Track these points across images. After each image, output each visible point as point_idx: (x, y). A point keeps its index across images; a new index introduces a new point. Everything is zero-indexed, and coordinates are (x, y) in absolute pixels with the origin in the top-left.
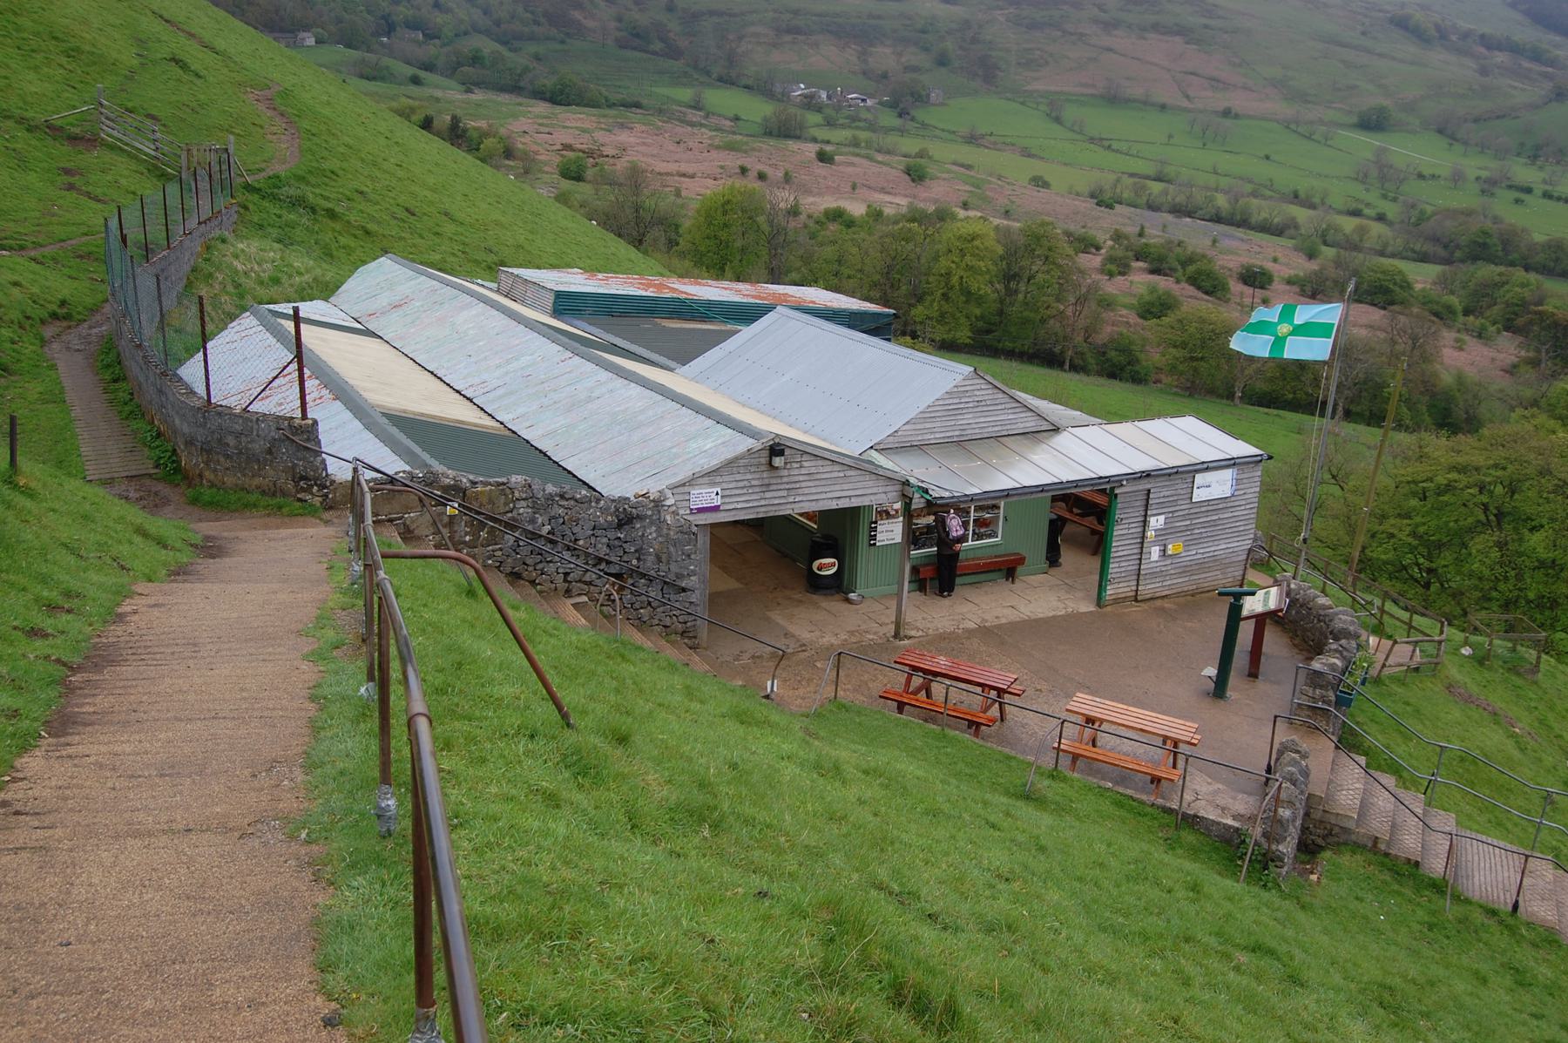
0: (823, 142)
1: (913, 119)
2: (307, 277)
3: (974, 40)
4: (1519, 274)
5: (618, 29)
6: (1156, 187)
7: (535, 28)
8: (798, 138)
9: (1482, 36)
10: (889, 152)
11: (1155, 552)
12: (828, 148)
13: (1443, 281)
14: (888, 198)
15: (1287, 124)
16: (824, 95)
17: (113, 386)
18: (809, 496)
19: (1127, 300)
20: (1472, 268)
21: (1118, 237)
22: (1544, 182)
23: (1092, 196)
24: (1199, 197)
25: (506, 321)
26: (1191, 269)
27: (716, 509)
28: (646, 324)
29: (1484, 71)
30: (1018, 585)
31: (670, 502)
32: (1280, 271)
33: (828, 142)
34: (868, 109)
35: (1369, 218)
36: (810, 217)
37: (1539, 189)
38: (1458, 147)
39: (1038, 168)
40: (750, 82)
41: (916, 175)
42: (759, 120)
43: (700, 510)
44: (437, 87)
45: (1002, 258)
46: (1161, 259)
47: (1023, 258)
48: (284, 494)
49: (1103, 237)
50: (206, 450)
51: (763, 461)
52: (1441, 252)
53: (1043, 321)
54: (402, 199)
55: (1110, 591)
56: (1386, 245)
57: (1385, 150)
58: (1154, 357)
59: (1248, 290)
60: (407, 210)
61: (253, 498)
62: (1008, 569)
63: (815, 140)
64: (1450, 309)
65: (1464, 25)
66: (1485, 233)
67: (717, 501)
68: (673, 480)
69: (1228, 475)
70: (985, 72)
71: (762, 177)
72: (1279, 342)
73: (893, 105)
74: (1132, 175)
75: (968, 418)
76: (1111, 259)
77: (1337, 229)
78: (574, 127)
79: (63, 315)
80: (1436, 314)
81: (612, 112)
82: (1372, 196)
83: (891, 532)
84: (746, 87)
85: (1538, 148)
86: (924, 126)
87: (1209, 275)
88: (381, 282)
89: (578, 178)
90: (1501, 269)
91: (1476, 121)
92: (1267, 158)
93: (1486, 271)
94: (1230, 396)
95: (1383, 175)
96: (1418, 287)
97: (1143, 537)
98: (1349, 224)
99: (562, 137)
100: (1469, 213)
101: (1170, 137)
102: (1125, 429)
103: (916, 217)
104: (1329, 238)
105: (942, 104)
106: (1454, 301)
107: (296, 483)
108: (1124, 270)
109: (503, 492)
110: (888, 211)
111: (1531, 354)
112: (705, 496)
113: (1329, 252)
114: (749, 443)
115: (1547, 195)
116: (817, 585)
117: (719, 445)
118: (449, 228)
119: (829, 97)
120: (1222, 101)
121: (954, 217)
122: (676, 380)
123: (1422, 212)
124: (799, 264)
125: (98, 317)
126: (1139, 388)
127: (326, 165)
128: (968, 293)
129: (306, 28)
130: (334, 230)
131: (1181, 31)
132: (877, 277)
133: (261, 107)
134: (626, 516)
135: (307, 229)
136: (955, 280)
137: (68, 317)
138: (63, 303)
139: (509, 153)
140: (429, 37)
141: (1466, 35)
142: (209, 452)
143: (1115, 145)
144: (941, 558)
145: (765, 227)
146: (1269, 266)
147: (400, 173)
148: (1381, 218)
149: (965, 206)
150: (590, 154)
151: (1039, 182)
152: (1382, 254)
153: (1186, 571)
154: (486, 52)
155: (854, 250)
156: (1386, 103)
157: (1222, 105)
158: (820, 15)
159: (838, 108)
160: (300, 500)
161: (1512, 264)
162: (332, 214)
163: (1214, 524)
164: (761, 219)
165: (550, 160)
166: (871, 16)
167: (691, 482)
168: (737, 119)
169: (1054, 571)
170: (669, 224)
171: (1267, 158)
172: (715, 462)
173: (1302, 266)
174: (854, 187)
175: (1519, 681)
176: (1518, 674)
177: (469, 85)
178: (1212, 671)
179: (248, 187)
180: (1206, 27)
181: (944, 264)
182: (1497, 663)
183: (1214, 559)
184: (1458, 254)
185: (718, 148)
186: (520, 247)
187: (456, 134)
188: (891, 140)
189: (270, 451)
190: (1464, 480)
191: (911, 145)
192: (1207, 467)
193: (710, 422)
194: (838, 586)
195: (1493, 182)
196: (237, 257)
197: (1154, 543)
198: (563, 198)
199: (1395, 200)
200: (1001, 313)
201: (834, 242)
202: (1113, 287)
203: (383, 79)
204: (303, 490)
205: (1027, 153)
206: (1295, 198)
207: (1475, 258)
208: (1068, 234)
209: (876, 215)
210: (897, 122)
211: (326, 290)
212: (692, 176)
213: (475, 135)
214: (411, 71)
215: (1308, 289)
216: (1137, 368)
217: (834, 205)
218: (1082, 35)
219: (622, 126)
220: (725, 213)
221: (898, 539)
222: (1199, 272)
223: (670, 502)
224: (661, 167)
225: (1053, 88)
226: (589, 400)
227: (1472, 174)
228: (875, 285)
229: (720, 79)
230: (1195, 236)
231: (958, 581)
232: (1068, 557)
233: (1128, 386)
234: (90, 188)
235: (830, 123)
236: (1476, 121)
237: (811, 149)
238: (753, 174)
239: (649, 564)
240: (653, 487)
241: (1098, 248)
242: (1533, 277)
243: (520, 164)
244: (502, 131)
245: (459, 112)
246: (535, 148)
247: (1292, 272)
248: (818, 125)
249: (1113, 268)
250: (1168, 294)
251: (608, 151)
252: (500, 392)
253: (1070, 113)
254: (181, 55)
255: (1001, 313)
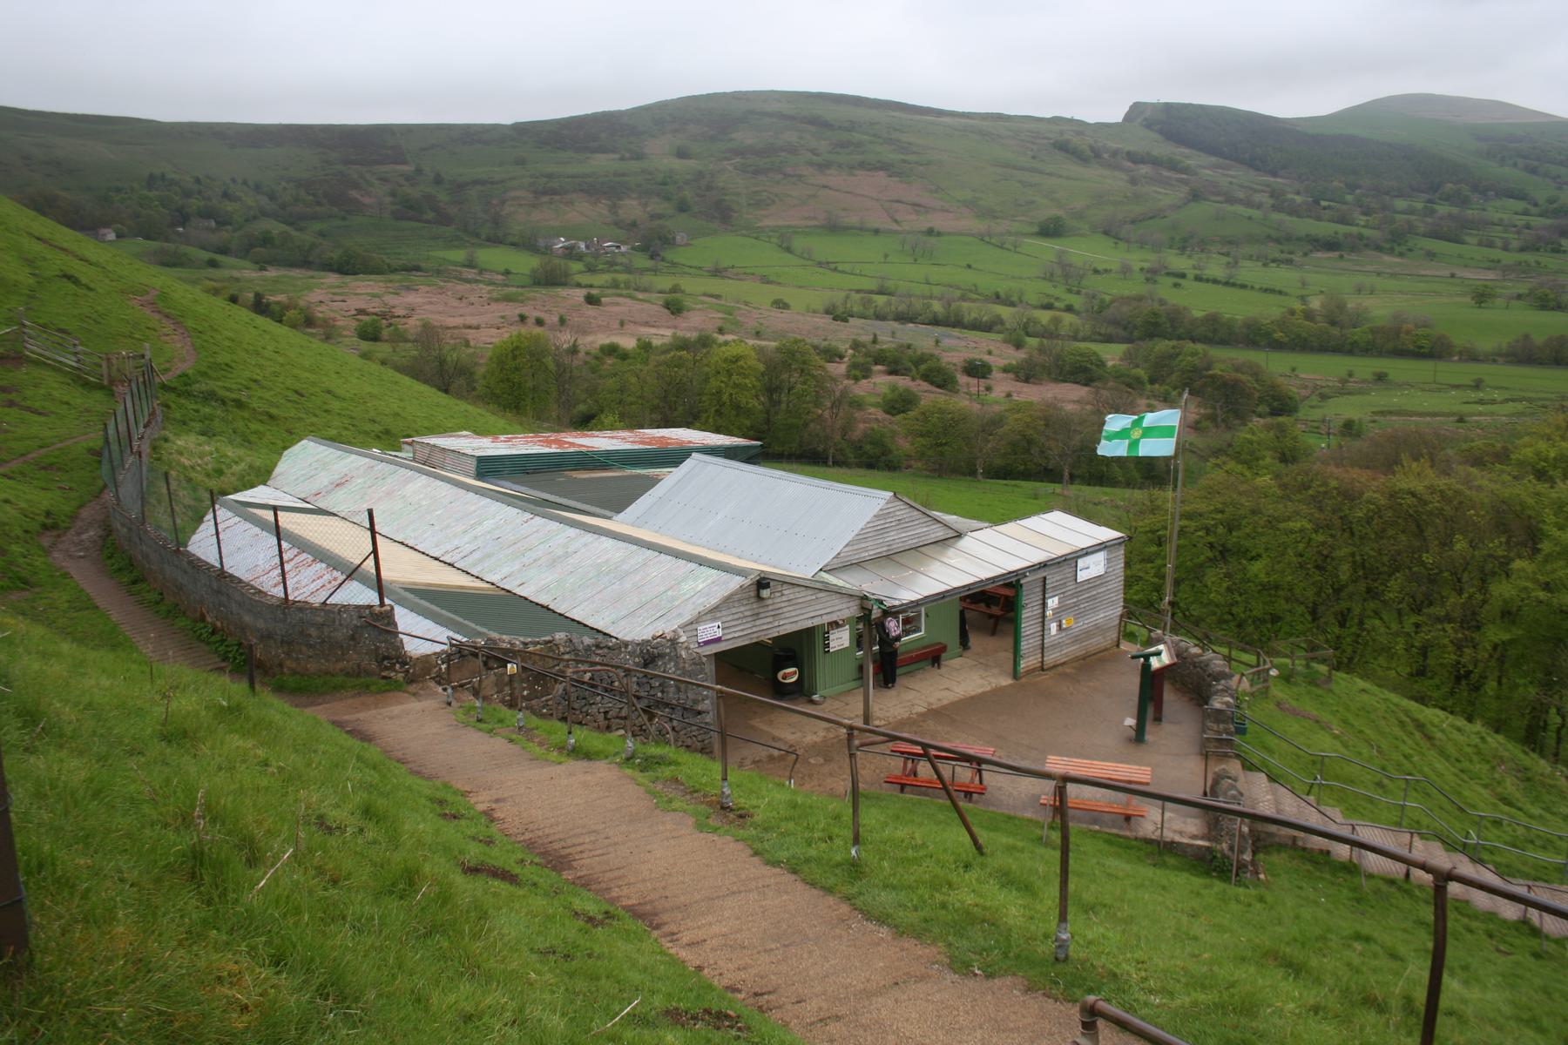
0: (587, 286)
1: (663, 260)
2: (242, 466)
3: (709, 188)
4: (1189, 346)
5: (393, 203)
6: (880, 300)
7: (318, 209)
8: (564, 284)
9: (1128, 153)
10: (646, 290)
11: (1054, 627)
12: (594, 292)
13: (1128, 357)
14: (653, 331)
15: (981, 237)
16: (582, 246)
17: (137, 587)
18: (791, 618)
19: (873, 400)
20: (1150, 344)
21: (856, 345)
22: (1194, 267)
23: (827, 312)
24: (918, 305)
25: (455, 490)
26: (923, 367)
27: (718, 640)
28: (560, 479)
29: (1133, 181)
30: (943, 670)
31: (683, 639)
32: (996, 362)
33: (591, 286)
34: (623, 254)
35: (1059, 310)
36: (587, 353)
37: (1191, 273)
38: (1122, 245)
39: (777, 292)
40: (515, 239)
41: (675, 308)
42: (527, 272)
43: (707, 643)
44: (233, 267)
45: (763, 374)
46: (896, 362)
47: (785, 370)
48: (368, 673)
49: (843, 347)
50: (287, 642)
51: (753, 594)
52: (1121, 332)
53: (806, 425)
54: (289, 382)
55: (1023, 664)
56: (1077, 331)
57: (1064, 252)
58: (904, 445)
59: (973, 381)
60: (296, 392)
61: (340, 679)
62: (933, 657)
63: (579, 285)
64: (1138, 380)
65: (1114, 145)
66: (1155, 314)
67: (719, 633)
68: (681, 621)
69: (1101, 557)
70: (722, 214)
71: (539, 322)
72: (1134, 444)
73: (644, 249)
74: (858, 291)
75: (892, 536)
76: (854, 366)
77: (1036, 322)
78: (365, 293)
79: (51, 525)
80: (1129, 385)
81: (397, 277)
82: (1060, 291)
83: (841, 639)
84: (513, 244)
85: (1185, 240)
86: (674, 264)
87: (939, 370)
88: (308, 466)
89: (375, 338)
90: (1173, 343)
91: (1133, 222)
92: (969, 266)
93: (1162, 346)
94: (972, 473)
95: (1066, 273)
96: (1110, 364)
97: (1044, 616)
98: (1044, 317)
99: (355, 303)
100: (1140, 299)
101: (886, 256)
102: (1010, 528)
103: (683, 345)
104: (1030, 330)
105: (687, 245)
106: (1140, 372)
107: (380, 663)
108: (866, 373)
109: (551, 649)
110: (656, 342)
111: (1209, 411)
112: (709, 630)
113: (1033, 342)
114: (736, 582)
115: (1198, 279)
116: (781, 691)
117: (708, 588)
118: (336, 405)
119: (587, 247)
120: (925, 222)
121: (714, 341)
122: (617, 524)
123: (1102, 301)
124: (584, 396)
125: (79, 523)
126: (896, 474)
127: (219, 359)
128: (737, 407)
129: (106, 225)
130: (243, 418)
131: (884, 167)
132: (656, 402)
133: (147, 311)
134: (651, 654)
135: (223, 419)
136: (725, 397)
137: (55, 527)
138: (48, 514)
139: (309, 322)
140: (222, 223)
141: (1115, 153)
142: (289, 643)
143: (840, 267)
144: (887, 650)
145: (552, 366)
146: (986, 358)
147: (281, 360)
148: (1069, 309)
149: (721, 331)
150: (383, 316)
151: (781, 305)
152: (1075, 338)
153: (1076, 640)
154: (275, 232)
155: (634, 380)
156: (1060, 213)
157: (925, 226)
158: (573, 177)
159: (596, 256)
160: (384, 678)
161: (1179, 338)
162: (239, 404)
163: (1093, 598)
164: (549, 361)
165: (348, 325)
166: (616, 174)
167: (697, 620)
168: (507, 273)
169: (967, 653)
170: (465, 371)
171: (969, 266)
172: (714, 601)
173: (1015, 357)
174: (622, 324)
175: (1320, 692)
176: (1317, 685)
177: (262, 264)
178: (1130, 721)
179: (164, 387)
180: (904, 161)
181: (714, 383)
182: (1300, 679)
183: (1097, 627)
184: (1136, 333)
185: (497, 300)
186: (397, 414)
187: (260, 307)
188: (646, 279)
189: (353, 638)
190: (1193, 525)
191: (665, 282)
192: (1086, 552)
193: (693, 566)
194: (802, 691)
195: (1154, 271)
196: (181, 454)
197: (1052, 621)
198: (365, 356)
199: (1078, 293)
200: (768, 421)
201: (615, 375)
202: (861, 389)
203: (182, 265)
204: (386, 668)
205: (765, 280)
206: (998, 298)
207: (1151, 336)
208: (815, 347)
209: (646, 347)
210: (649, 263)
211: (262, 475)
212: (478, 328)
213: (277, 308)
214: (206, 255)
215: (1022, 375)
216: (890, 457)
217: (607, 341)
218: (801, 176)
219: (408, 288)
220: (515, 358)
221: (847, 644)
222: (930, 370)
223: (683, 639)
224: (451, 322)
225: (781, 223)
226: (567, 555)
227: (1136, 266)
228: (654, 409)
229: (489, 240)
230: (921, 338)
231: (899, 671)
232: (975, 640)
233: (886, 473)
234: (29, 403)
235: (591, 270)
236: (1133, 222)
237: (579, 294)
238: (531, 321)
239: (671, 695)
240: (666, 627)
241: (841, 357)
242: (1199, 347)
243: (321, 331)
244: (302, 303)
245: (258, 289)
246: (332, 315)
247: (1006, 362)
248: (581, 272)
249: (858, 373)
250: (907, 390)
251: (401, 312)
252: (477, 555)
253: (799, 243)
254: (71, 272)
255: (768, 421)
